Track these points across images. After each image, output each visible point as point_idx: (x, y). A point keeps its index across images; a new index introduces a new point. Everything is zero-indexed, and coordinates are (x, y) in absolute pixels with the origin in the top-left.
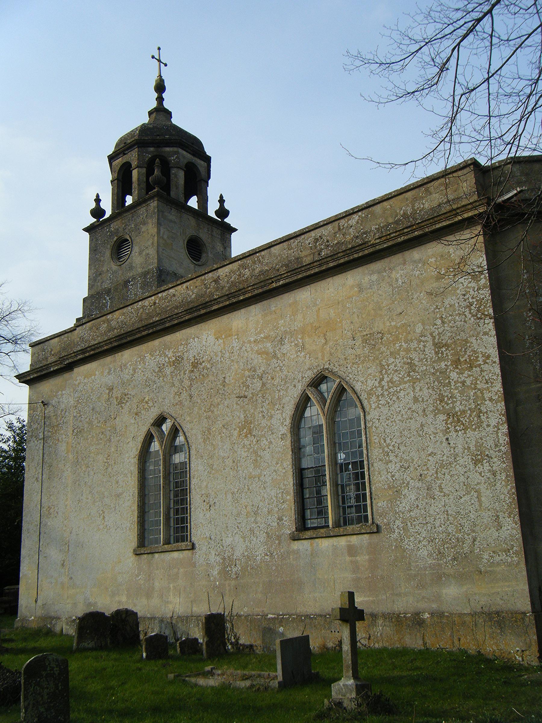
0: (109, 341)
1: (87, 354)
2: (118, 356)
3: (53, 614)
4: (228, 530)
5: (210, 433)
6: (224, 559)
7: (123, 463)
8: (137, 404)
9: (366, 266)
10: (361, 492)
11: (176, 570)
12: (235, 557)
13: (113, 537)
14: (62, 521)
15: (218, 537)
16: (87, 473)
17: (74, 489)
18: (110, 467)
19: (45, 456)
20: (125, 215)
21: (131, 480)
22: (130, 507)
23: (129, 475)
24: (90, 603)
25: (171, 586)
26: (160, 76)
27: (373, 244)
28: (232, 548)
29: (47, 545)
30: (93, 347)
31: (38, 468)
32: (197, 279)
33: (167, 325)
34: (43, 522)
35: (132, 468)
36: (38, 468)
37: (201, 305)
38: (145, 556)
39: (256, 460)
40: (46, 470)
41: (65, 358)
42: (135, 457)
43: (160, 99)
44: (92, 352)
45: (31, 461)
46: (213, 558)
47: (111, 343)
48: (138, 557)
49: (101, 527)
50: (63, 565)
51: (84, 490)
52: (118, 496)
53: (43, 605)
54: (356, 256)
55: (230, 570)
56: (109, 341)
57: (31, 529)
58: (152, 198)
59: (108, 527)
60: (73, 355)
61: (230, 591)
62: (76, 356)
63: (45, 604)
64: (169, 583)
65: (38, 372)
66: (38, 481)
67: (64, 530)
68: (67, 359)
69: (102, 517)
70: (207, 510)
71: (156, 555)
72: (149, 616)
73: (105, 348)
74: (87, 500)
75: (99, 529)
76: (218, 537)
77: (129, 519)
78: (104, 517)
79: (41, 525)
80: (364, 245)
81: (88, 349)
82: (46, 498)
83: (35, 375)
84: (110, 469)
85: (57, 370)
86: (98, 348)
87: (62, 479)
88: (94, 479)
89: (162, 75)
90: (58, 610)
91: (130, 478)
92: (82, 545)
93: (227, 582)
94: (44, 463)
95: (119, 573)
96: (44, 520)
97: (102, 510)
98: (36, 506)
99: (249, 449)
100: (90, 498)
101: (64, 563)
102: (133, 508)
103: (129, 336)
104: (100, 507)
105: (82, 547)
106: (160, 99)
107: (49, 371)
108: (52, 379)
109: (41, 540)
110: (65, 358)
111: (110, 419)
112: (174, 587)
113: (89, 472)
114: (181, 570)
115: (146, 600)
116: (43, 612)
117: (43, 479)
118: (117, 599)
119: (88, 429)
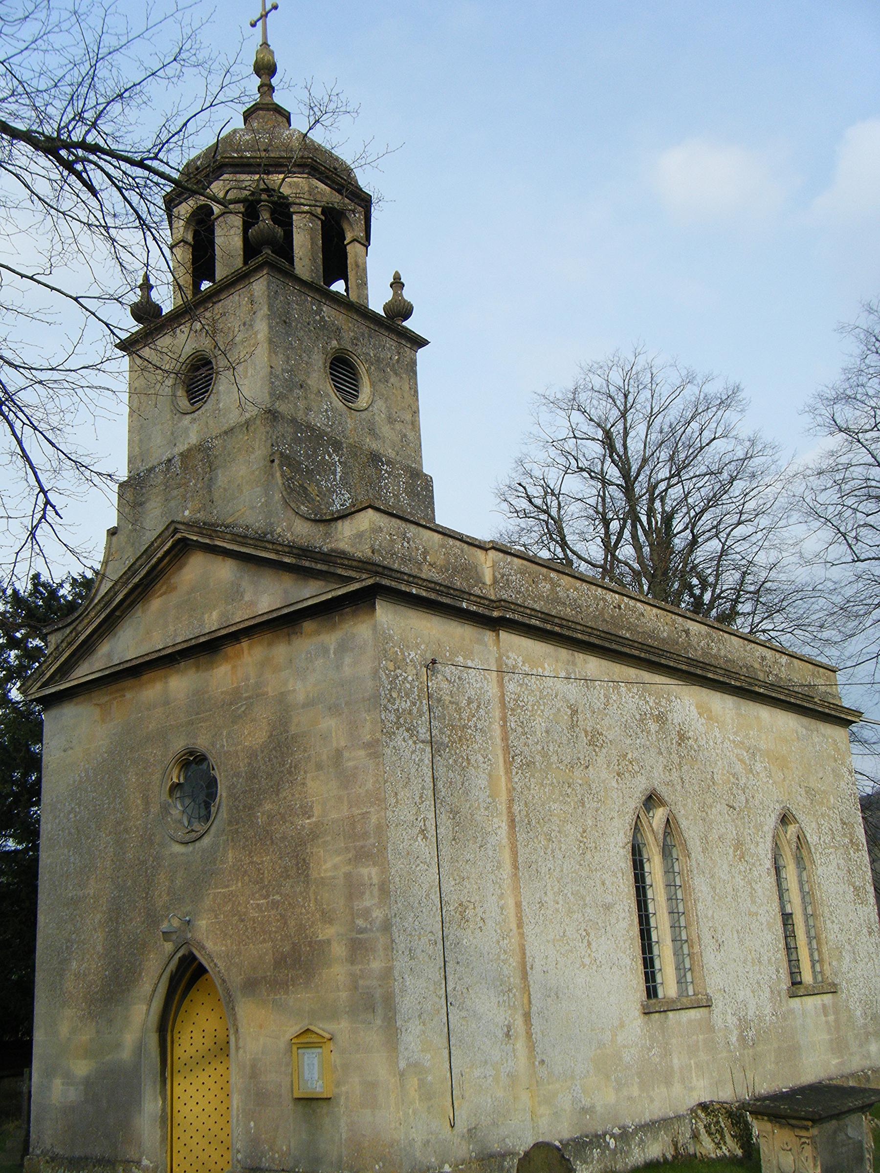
0: (590, 631)
1: (549, 627)
2: (580, 657)
3: (496, 1148)
4: (739, 981)
5: (708, 843)
6: (740, 1020)
7: (608, 851)
8: (618, 758)
9: (810, 719)
10: (648, 956)
11: (695, 1037)
12: (749, 1018)
13: (608, 982)
14: (494, 939)
15: (732, 990)
16: (549, 851)
17: (527, 877)
18: (589, 852)
19: (440, 785)
20: (355, 317)
21: (624, 884)
22: (627, 932)
23: (620, 875)
24: (583, 1108)
25: (692, 1062)
26: (265, 44)
27: (815, 702)
28: (745, 1006)
29: (465, 991)
30: (564, 623)
31: (423, 807)
32: (668, 614)
33: (710, 675)
34: (451, 937)
35: (623, 865)
36: (423, 807)
37: (803, 694)
38: (657, 1015)
39: (751, 893)
40: (443, 816)
41: (513, 607)
42: (624, 847)
43: (267, 89)
44: (557, 629)
45: (401, 784)
46: (732, 1021)
47: (590, 634)
48: (647, 1017)
49: (587, 960)
50: (508, 1035)
51: (549, 884)
52: (608, 907)
53: (469, 1130)
54: (792, 700)
55: (747, 1035)
56: (590, 631)
57: (419, 951)
58: (258, 268)
59: (598, 962)
60: (528, 611)
61: (749, 1062)
62: (530, 616)
63: (475, 1128)
64: (690, 1059)
65: (433, 590)
66: (425, 837)
67: (503, 961)
68: (514, 611)
69: (585, 942)
70: (717, 950)
71: (670, 1014)
72: (672, 1115)
73: (579, 636)
74: (557, 906)
75: (584, 965)
76: (732, 990)
77: (628, 952)
78: (589, 944)
79: (447, 944)
80: (809, 698)
81: (556, 620)
82: (453, 883)
83: (424, 594)
84: (588, 856)
85: (474, 613)
86: (569, 628)
87: (486, 849)
88: (565, 866)
89: (269, 43)
90: (508, 1136)
91: (621, 881)
92: (557, 994)
93: (746, 1052)
94: (438, 801)
95: (624, 1046)
96: (452, 932)
97: (585, 930)
98: (428, 895)
99: (745, 877)
100: (561, 902)
101: (509, 1031)
102: (631, 933)
103: (647, 652)
104: (580, 923)
105: (558, 997)
106: (267, 89)
107: (458, 604)
108: (438, 618)
109: (450, 978)
110: (513, 607)
111: (579, 764)
112: (695, 1063)
113: (553, 851)
114: (701, 1037)
115: (665, 1089)
116: (471, 1147)
117: (440, 837)
118: (625, 1093)
119: (543, 767)
